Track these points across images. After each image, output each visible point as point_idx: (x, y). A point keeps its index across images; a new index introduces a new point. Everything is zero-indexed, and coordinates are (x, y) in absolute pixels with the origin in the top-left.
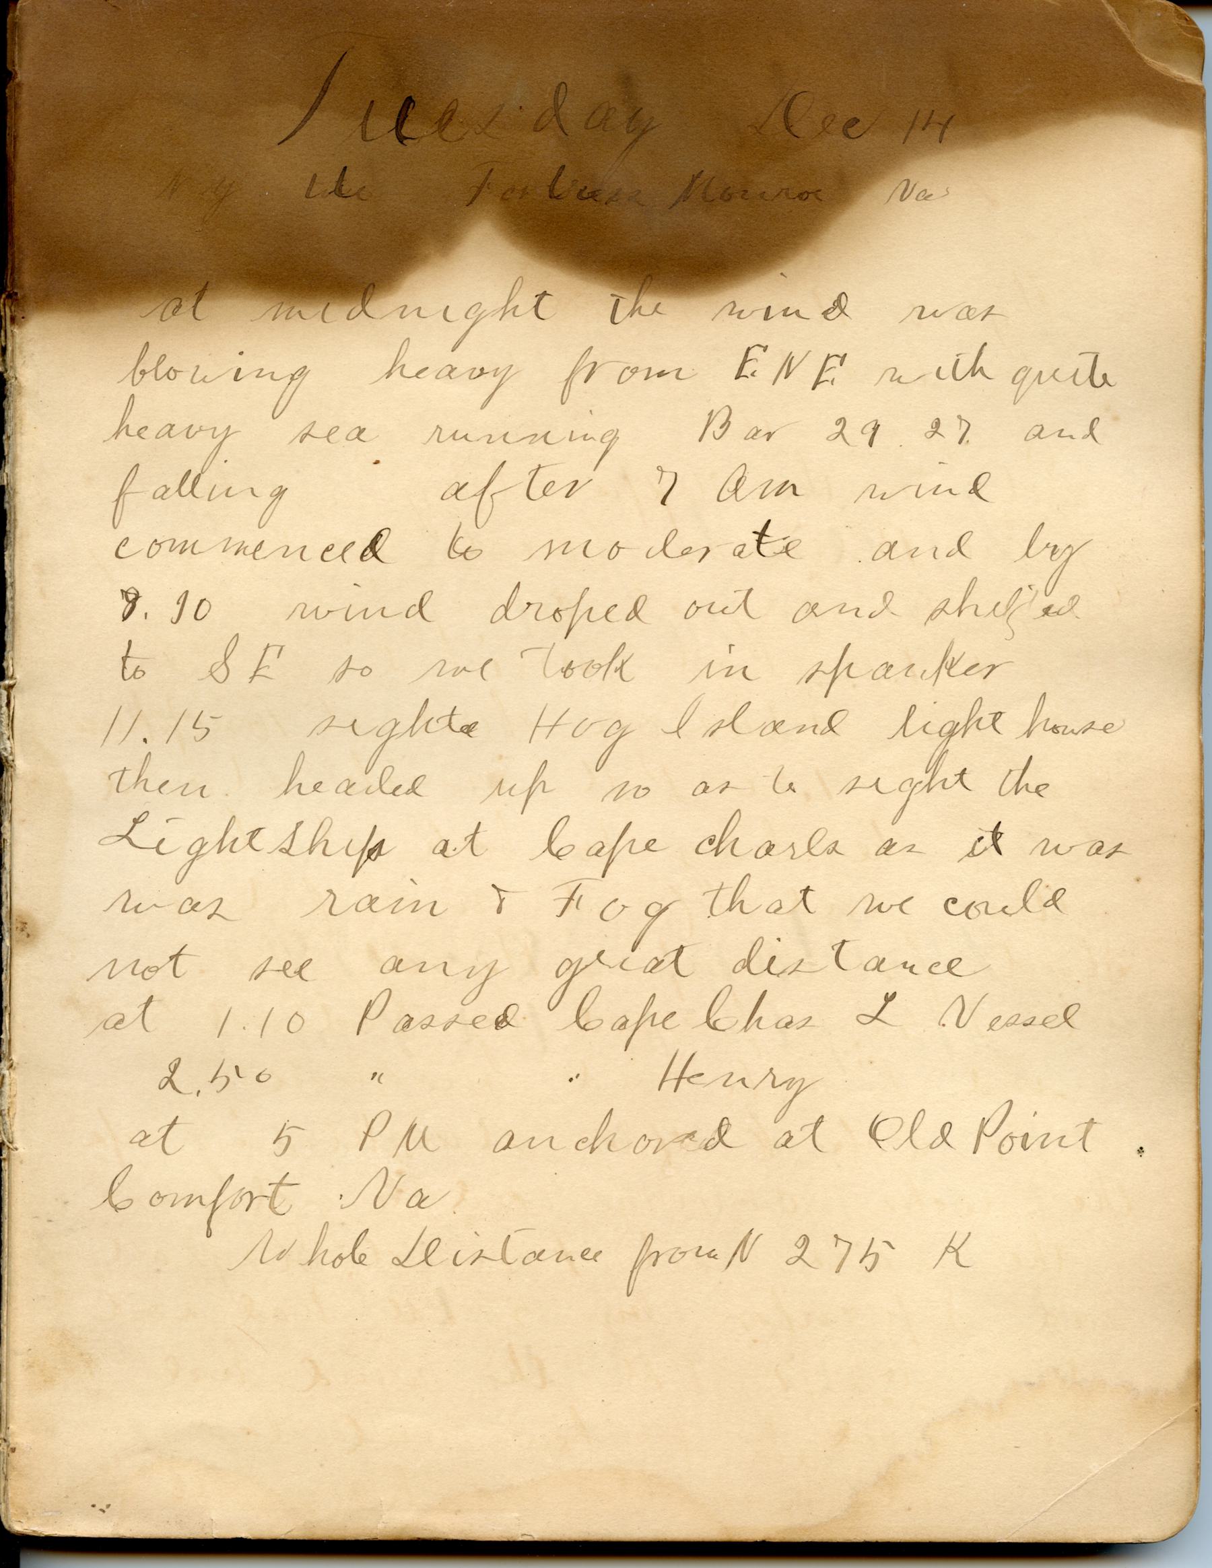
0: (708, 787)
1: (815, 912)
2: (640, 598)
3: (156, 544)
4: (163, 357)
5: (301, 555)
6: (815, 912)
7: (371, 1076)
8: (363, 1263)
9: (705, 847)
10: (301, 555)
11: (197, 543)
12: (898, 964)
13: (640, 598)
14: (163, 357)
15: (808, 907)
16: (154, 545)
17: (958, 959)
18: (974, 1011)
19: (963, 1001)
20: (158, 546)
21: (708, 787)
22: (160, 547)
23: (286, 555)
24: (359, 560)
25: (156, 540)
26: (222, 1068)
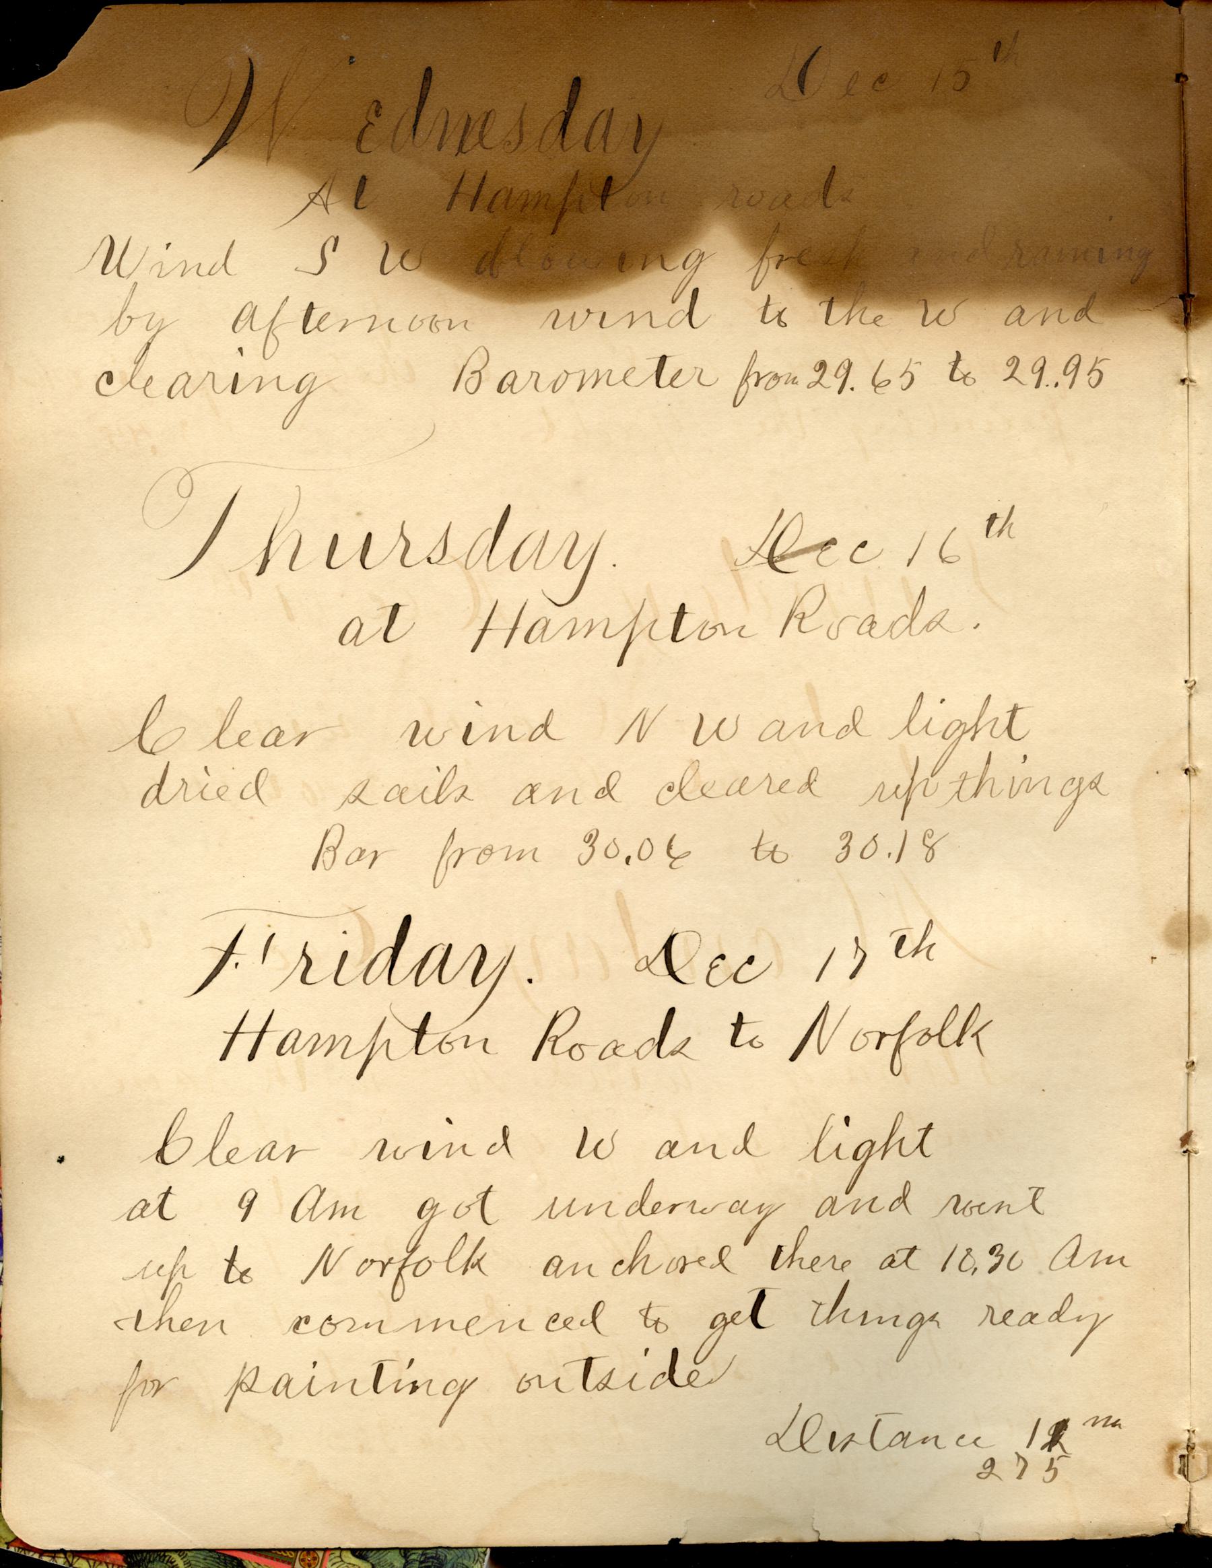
0: (149, 1204)
1: (1014, 537)
2: (283, 1376)
3: (331, 1324)
4: (817, 1260)
5: (286, 1394)
6: (1014, 537)
7: (313, 1366)
8: (569, 1326)
9: (666, 796)
10: (286, 1394)
11: (399, 1150)
12: (387, 604)
13: (283, 1376)
14: (817, 1260)
15: (783, 570)
16: (326, 1323)
17: (1077, 1236)
18: (520, 793)
19: (651, 316)
20: (333, 1327)
21: (149, 1204)
22: (336, 1328)
23: (819, 1215)
24: (954, 1214)
25: (329, 1318)
26: (1080, 1250)
